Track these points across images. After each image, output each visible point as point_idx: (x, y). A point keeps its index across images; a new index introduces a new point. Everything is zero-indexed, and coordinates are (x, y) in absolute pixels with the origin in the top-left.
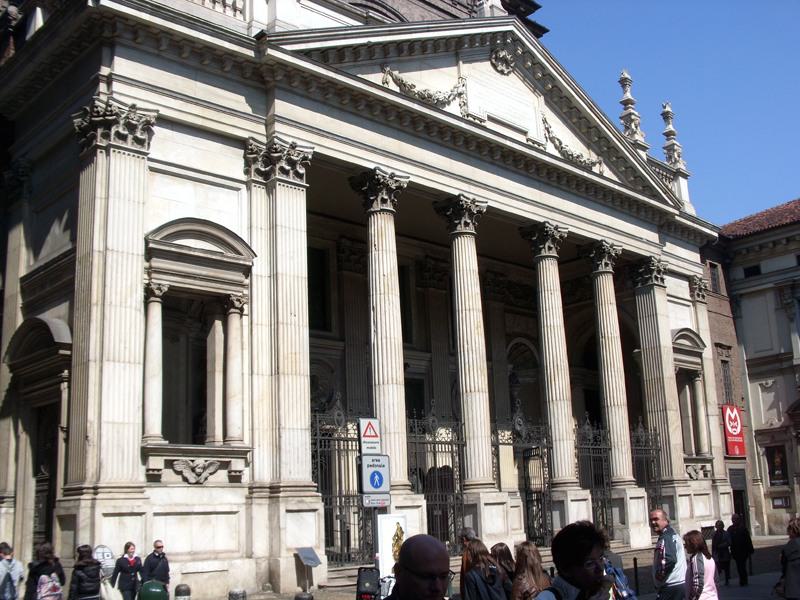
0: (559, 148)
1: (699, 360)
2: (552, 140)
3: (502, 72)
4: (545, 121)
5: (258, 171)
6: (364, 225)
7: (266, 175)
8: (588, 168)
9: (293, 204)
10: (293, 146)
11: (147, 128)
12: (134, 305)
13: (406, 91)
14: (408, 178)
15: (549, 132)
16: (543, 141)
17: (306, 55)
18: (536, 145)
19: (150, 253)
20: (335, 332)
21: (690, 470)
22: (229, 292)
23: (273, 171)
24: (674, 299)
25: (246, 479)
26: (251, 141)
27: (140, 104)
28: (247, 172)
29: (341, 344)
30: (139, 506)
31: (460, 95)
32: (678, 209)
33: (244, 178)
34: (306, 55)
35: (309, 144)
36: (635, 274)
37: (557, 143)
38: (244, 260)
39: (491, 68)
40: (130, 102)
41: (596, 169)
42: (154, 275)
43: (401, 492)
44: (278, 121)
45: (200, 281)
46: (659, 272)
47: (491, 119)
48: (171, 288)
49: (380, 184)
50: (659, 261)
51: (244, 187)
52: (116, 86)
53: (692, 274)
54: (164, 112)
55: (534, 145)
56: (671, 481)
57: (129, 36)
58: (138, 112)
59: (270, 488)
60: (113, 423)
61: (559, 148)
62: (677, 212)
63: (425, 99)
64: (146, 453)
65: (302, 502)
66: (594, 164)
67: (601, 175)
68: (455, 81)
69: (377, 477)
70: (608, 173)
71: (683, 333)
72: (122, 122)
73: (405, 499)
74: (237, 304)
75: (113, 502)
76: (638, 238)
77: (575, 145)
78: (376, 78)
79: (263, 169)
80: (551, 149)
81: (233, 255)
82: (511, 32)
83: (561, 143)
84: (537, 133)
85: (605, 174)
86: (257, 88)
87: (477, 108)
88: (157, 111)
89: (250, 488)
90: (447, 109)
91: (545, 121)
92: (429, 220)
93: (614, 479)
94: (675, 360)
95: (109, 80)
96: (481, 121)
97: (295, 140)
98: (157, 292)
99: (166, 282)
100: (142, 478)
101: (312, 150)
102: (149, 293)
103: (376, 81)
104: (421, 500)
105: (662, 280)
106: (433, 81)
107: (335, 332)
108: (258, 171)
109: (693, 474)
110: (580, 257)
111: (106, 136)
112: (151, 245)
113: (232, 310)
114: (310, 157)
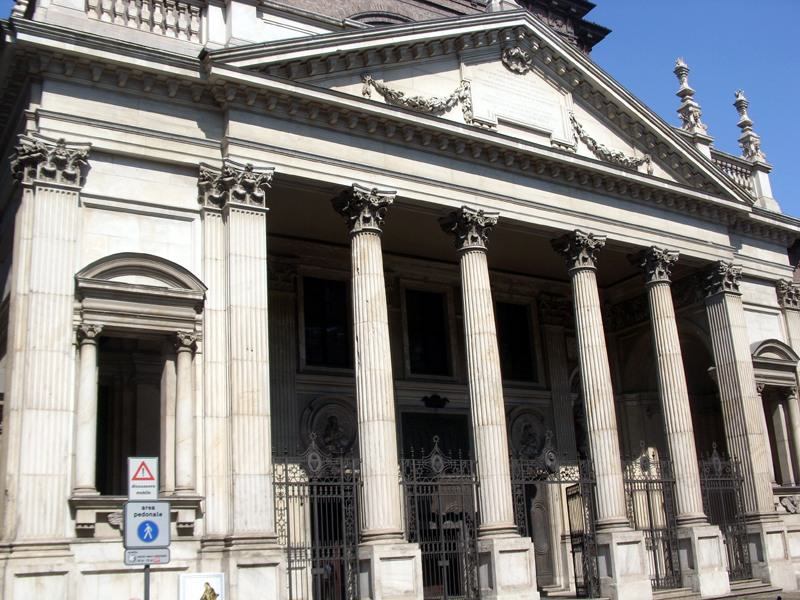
0: (594, 148)
1: (792, 375)
2: (584, 140)
3: (517, 71)
4: (573, 120)
5: (212, 199)
6: (347, 247)
7: (221, 202)
8: (632, 168)
9: (250, 232)
10: (249, 169)
11: (81, 163)
12: (62, 348)
13: (393, 100)
14: (395, 192)
15: (579, 132)
16: (573, 143)
17: (263, 70)
18: (563, 148)
19: (81, 293)
20: (542, 383)
21: (786, 501)
22: (177, 330)
23: (226, 197)
24: (751, 306)
25: (198, 532)
26: (202, 167)
27: (68, 138)
28: (201, 201)
29: (548, 393)
30: (59, 565)
31: (462, 99)
32: (751, 205)
33: (197, 207)
34: (263, 70)
35: (267, 164)
36: (700, 285)
37: (590, 143)
38: (193, 294)
39: (504, 69)
40: (58, 136)
41: (643, 169)
42: (86, 316)
43: (390, 541)
44: (232, 143)
45: (139, 319)
46: (731, 277)
47: (501, 122)
48: (106, 329)
49: (361, 201)
50: (730, 266)
51: (197, 217)
52: (43, 122)
53: (778, 278)
54: (97, 144)
55: (561, 147)
56: (757, 516)
57: (57, 69)
58: (67, 146)
59: (225, 540)
60: (35, 475)
61: (594, 148)
62: (749, 209)
63: (416, 107)
64: (75, 506)
65: (258, 555)
66: (640, 163)
67: (649, 175)
68: (457, 85)
69: (149, 529)
70: (658, 171)
71: (770, 345)
72: (49, 159)
73: (393, 549)
74: (187, 342)
75: (28, 561)
76: (705, 243)
77: (613, 143)
78: (355, 89)
79: (217, 196)
80: (583, 150)
81: (183, 290)
82: (523, 26)
83: (594, 143)
84: (563, 133)
85: (656, 174)
86: (209, 111)
87: (484, 111)
88: (89, 144)
89: (202, 541)
90: (446, 116)
91: (573, 120)
92: (424, 243)
93: (681, 517)
94: (756, 376)
95: (36, 117)
96: (490, 125)
97: (62, 136)
98: (90, 334)
99: (100, 322)
100: (70, 533)
101: (272, 172)
102: (81, 336)
103: (357, 93)
104: (416, 550)
105: (736, 287)
106: (427, 87)
107: (542, 383)
108: (212, 199)
109: (790, 507)
110: (626, 273)
111: (33, 174)
112: (81, 284)
113: (181, 348)
114: (270, 178)
